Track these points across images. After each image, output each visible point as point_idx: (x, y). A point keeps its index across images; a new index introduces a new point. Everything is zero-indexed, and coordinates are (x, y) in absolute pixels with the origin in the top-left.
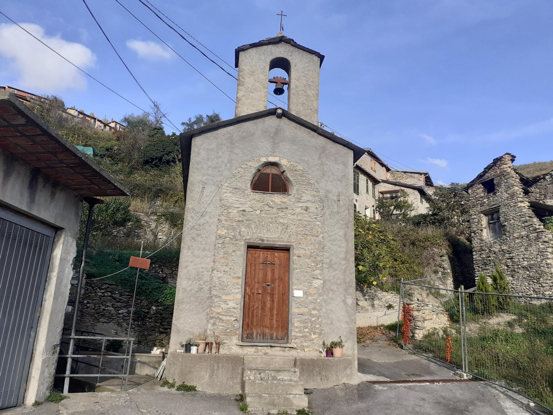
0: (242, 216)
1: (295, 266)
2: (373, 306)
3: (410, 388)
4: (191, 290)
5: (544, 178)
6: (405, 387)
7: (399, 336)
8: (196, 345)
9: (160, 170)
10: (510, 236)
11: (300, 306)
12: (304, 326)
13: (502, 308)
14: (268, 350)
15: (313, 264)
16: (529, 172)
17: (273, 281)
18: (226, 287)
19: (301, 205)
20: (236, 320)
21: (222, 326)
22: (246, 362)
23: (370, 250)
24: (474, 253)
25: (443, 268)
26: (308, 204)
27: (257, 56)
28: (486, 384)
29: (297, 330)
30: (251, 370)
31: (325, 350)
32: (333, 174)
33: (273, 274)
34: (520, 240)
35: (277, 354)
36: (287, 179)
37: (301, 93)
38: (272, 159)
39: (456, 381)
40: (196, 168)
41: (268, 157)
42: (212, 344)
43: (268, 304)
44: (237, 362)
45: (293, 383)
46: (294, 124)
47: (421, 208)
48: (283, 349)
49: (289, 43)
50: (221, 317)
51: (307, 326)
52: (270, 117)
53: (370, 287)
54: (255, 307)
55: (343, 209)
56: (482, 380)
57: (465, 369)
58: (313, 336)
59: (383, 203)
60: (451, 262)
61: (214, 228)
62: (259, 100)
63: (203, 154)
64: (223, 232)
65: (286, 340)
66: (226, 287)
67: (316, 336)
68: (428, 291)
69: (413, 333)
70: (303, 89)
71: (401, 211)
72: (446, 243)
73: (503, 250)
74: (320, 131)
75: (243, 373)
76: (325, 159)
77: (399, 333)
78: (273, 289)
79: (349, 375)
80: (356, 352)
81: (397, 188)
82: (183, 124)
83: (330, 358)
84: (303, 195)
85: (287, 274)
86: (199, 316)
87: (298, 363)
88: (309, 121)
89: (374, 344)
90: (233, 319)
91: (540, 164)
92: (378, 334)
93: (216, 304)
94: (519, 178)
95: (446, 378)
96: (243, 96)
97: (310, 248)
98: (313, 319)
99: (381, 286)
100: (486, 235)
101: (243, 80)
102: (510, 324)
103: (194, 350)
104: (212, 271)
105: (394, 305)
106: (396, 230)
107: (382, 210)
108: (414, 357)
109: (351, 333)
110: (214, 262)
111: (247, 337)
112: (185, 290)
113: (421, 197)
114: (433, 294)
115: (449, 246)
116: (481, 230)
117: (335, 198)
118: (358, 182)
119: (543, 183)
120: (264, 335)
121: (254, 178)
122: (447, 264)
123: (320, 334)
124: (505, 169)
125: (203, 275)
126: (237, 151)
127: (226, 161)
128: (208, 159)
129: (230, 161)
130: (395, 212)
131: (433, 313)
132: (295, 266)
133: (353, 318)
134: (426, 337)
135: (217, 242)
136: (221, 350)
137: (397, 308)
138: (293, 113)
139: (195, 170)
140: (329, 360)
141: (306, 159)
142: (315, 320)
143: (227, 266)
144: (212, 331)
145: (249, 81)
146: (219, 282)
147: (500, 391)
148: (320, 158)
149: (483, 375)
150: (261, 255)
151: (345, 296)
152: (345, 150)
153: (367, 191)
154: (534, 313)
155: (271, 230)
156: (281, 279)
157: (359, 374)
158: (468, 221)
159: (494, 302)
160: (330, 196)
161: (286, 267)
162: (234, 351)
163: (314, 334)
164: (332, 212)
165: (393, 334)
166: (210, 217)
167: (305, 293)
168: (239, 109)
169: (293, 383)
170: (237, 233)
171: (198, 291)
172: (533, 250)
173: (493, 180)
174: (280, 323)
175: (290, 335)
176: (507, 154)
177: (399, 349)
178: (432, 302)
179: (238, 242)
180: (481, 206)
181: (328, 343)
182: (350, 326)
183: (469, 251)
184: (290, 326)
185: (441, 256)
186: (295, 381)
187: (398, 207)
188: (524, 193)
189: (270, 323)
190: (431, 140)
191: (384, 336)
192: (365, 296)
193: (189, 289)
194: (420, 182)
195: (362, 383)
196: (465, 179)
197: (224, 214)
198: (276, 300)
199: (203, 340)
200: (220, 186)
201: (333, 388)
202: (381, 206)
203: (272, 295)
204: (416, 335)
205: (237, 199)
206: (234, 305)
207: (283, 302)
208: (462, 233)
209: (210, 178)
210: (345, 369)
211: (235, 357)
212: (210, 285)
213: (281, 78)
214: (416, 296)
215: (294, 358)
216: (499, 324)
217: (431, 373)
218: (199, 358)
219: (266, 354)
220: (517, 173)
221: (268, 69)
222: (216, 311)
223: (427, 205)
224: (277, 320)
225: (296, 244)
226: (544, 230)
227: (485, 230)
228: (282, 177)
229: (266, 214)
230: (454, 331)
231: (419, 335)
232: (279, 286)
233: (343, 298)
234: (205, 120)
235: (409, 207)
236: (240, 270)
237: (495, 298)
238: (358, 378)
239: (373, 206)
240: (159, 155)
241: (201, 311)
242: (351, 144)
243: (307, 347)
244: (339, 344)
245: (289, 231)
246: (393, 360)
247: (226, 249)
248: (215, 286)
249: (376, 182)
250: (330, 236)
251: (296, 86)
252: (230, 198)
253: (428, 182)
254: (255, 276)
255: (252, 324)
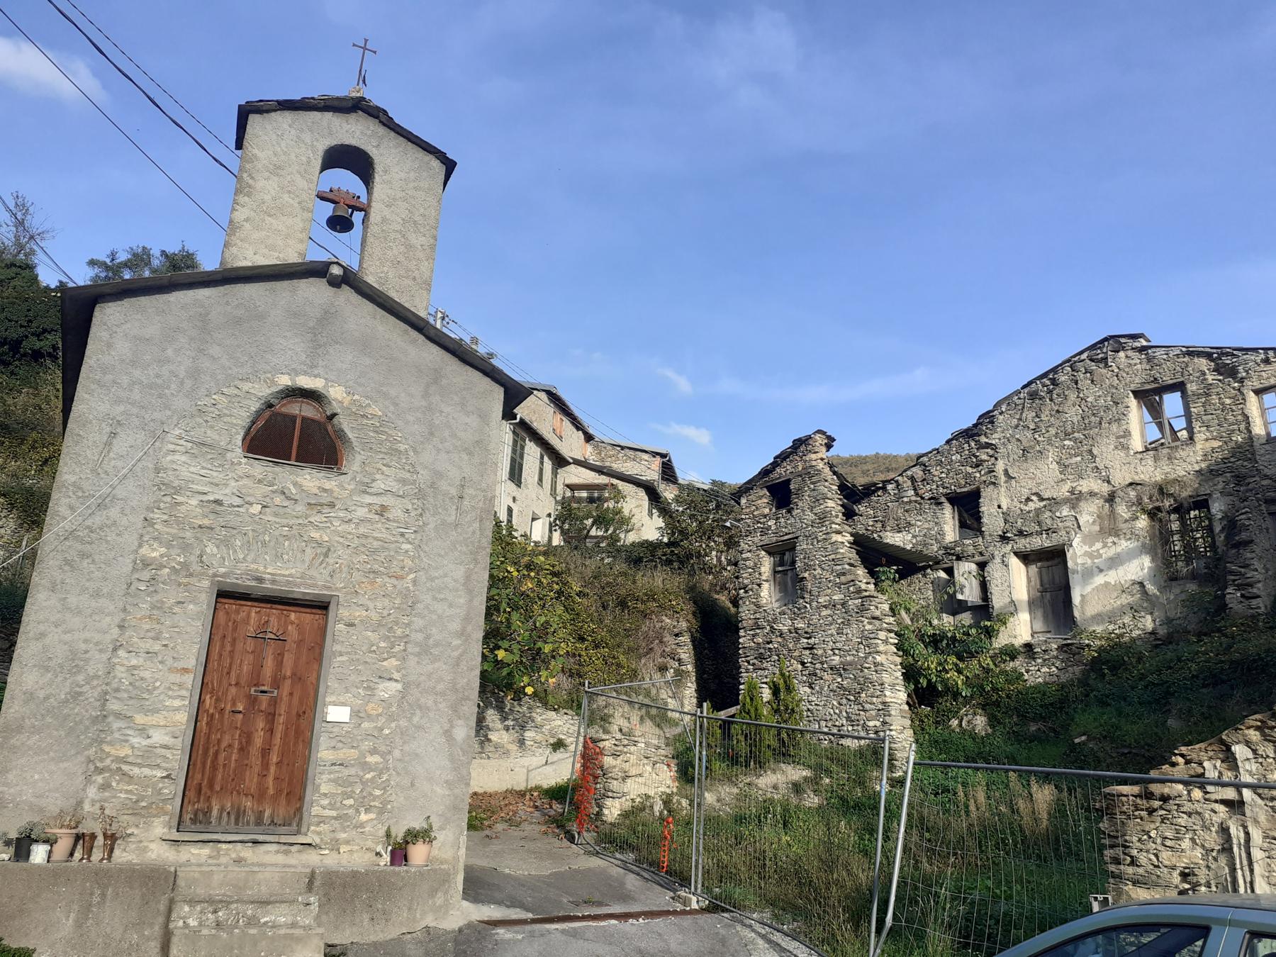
0: (212, 516)
1: (337, 648)
2: (522, 742)
3: (574, 934)
4: (47, 698)
5: (884, 488)
6: (563, 931)
7: (569, 812)
8: (46, 841)
9: (12, 373)
10: (812, 600)
11: (340, 745)
12: (344, 793)
13: (785, 752)
14: (247, 852)
15: (382, 644)
16: (865, 473)
17: (276, 683)
18: (150, 692)
19: (368, 499)
20: (168, 777)
21: (127, 792)
22: (181, 882)
23: (528, 616)
24: (742, 633)
25: (679, 660)
26: (387, 500)
27: (293, 132)
28: (733, 919)
29: (325, 802)
30: (192, 902)
31: (390, 848)
32: (454, 435)
33: (279, 664)
34: (829, 612)
35: (270, 861)
36: (341, 434)
37: (393, 236)
38: (305, 382)
39: (675, 913)
40: (98, 382)
41: (297, 375)
42: (93, 837)
43: (258, 739)
44: (159, 885)
45: (298, 932)
46: (369, 307)
47: (647, 527)
48: (286, 847)
49: (377, 117)
50: (125, 768)
51: (353, 792)
52: (311, 280)
53: (520, 699)
54: (224, 745)
55: (468, 519)
56: (724, 910)
57: (696, 888)
58: (364, 817)
59: (570, 510)
60: (694, 649)
61: (131, 540)
62: (287, 236)
63: (123, 347)
64: (154, 552)
65: (295, 827)
66: (150, 692)
67: (372, 816)
68: (644, 711)
69: (599, 806)
70: (398, 227)
71: (607, 531)
72: (689, 607)
73: (796, 629)
74: (432, 333)
75: (170, 911)
76: (438, 398)
77: (568, 807)
78: (274, 702)
79: (440, 907)
80: (463, 851)
81: (603, 480)
82: (92, 263)
83: (397, 869)
84: (378, 476)
85: (316, 667)
86: (66, 765)
87: (317, 883)
88: (406, 305)
89: (514, 832)
90: (159, 774)
91: (886, 457)
92: (524, 809)
93: (117, 735)
94: (837, 482)
95: (655, 909)
96: (247, 220)
97: (379, 605)
98: (368, 776)
99: (542, 698)
100: (768, 594)
101: (251, 182)
102: (797, 788)
103: (39, 853)
104: (115, 650)
105: (569, 740)
106: (589, 573)
107: (566, 526)
108: (595, 862)
109: (455, 808)
110: (121, 627)
111: (194, 821)
112: (30, 696)
113: (651, 504)
114: (652, 718)
115: (694, 614)
116: (759, 585)
117: (454, 492)
118: (522, 457)
119: (879, 499)
120: (239, 814)
121: (253, 423)
122: (686, 654)
123: (381, 811)
124: (814, 463)
125: (87, 661)
126: (215, 350)
127: (182, 374)
128: (133, 363)
129: (195, 374)
130: (593, 532)
131: (645, 761)
132: (337, 648)
133: (464, 772)
134: (625, 815)
135: (136, 576)
136: (117, 852)
137: (572, 748)
138: (371, 280)
139: (93, 386)
140: (394, 873)
141: (393, 392)
142: (374, 777)
143: (156, 638)
144: (98, 805)
145: (266, 187)
146: (131, 679)
147: (759, 934)
148: (426, 395)
149: (728, 898)
150: (253, 615)
151: (450, 721)
152: (486, 383)
153: (541, 479)
154: (844, 765)
155: (286, 557)
156: (297, 678)
157: (465, 904)
158: (736, 564)
159: (770, 739)
160: (443, 485)
161: (315, 649)
162: (153, 856)
163: (367, 811)
164: (444, 523)
165: (557, 807)
166: (122, 512)
167: (355, 714)
168: (234, 250)
169: (298, 932)
170: (193, 558)
171: (67, 701)
172: (852, 632)
173: (788, 481)
174: (285, 785)
175: (305, 814)
176: (819, 432)
177: (566, 843)
178: (649, 736)
179: (193, 580)
180: (763, 533)
181: (399, 833)
182: (456, 791)
183: (731, 626)
184: (308, 792)
185: (677, 635)
186: (304, 927)
187: (600, 521)
188: (844, 514)
189: (259, 783)
190: (684, 385)
191: (537, 814)
192: (506, 719)
193: (41, 694)
194: (650, 471)
195: (470, 925)
196: (738, 476)
197: (162, 505)
198: (279, 729)
199: (69, 827)
200: (158, 433)
201: (398, 941)
202: (567, 516)
203: (271, 717)
204: (606, 811)
205: (203, 472)
206: (167, 740)
207: (298, 733)
208: (724, 587)
209: (135, 410)
210: (433, 893)
211: (152, 871)
212: (104, 687)
213: (348, 192)
214: (618, 721)
215: (308, 870)
216: (775, 787)
217: (625, 897)
218: (51, 874)
219: (238, 861)
220: (835, 473)
221: (318, 168)
222: (113, 752)
223: (660, 522)
224: (276, 779)
225: (347, 593)
226: (875, 594)
227: (766, 586)
228: (329, 428)
229: (276, 515)
230: (685, 803)
231: (613, 810)
232: (291, 694)
233: (447, 726)
234: (156, 263)
235: (624, 522)
236: (191, 653)
237: (773, 732)
238: (462, 913)
239: (549, 515)
240: (14, 334)
241: (73, 752)
242: (501, 372)
243: (347, 842)
244: (424, 835)
245: (331, 560)
246: (546, 869)
247: (157, 597)
248: (117, 690)
249: (560, 461)
250: (432, 579)
251: (384, 220)
252: (184, 466)
253: (668, 472)
254: (230, 668)
255: (211, 786)
